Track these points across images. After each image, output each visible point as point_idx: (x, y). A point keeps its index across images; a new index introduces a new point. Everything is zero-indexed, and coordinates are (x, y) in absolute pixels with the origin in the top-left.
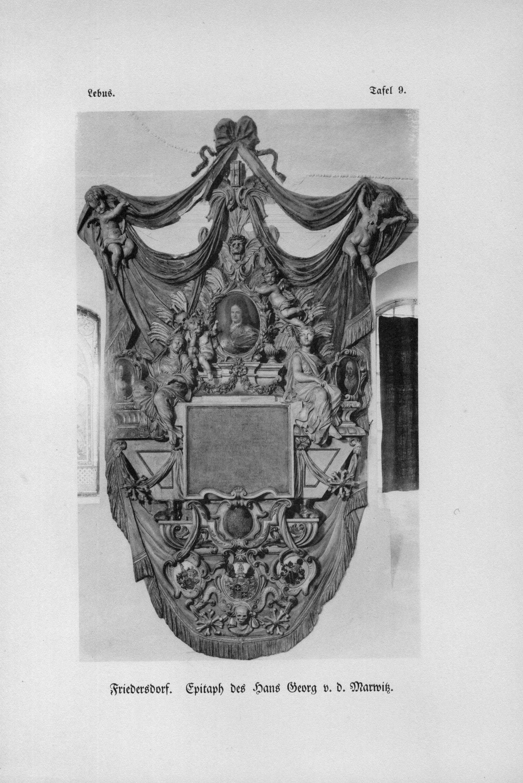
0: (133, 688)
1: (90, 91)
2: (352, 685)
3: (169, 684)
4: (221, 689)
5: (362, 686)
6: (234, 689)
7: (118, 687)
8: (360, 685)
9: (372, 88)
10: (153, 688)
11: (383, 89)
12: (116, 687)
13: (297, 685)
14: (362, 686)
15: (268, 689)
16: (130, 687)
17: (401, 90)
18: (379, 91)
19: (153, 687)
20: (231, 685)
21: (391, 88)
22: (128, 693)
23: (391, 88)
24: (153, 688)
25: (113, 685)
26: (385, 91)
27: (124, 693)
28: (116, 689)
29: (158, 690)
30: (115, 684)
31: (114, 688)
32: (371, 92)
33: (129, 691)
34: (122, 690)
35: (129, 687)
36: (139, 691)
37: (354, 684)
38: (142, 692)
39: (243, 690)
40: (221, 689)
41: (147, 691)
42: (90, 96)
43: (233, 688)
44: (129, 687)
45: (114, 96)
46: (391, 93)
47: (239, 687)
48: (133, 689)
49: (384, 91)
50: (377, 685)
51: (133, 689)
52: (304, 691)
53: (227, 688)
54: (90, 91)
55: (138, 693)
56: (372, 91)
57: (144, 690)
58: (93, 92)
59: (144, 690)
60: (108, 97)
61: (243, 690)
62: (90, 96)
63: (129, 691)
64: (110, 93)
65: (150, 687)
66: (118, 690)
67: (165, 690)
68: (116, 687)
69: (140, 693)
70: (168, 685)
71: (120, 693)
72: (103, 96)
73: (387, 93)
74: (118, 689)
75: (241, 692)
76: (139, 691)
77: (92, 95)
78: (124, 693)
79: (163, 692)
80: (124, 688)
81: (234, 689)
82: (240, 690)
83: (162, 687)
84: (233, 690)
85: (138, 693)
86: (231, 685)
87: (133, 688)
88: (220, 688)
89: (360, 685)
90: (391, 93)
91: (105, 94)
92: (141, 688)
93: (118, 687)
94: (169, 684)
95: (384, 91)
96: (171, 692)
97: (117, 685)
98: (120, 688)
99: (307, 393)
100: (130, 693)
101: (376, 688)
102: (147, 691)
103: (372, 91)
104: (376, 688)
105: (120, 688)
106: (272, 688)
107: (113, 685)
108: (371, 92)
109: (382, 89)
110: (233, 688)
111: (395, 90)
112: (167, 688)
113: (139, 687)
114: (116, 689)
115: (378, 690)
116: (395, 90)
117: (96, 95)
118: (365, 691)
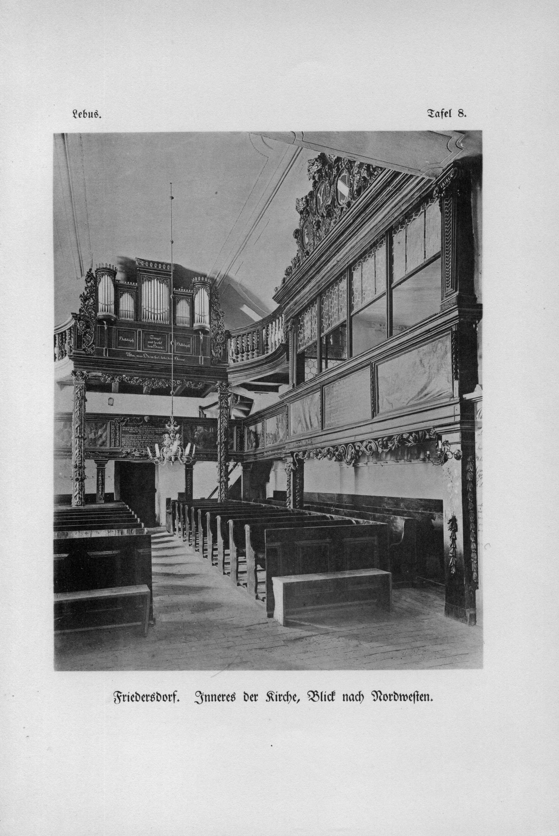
0: (138, 697)
1: (75, 111)
2: (374, 693)
3: (176, 691)
4: (361, 697)
5: (381, 694)
6: (254, 697)
7: (122, 694)
8: (379, 693)
9: (430, 111)
10: (159, 696)
11: (442, 112)
12: (119, 695)
13: (420, 694)
14: (381, 694)
15: (324, 697)
16: (135, 695)
17: (461, 113)
18: (437, 114)
19: (139, 695)
20: (245, 693)
21: (450, 111)
22: (133, 701)
23: (450, 111)
24: (159, 696)
25: (117, 693)
26: (444, 114)
27: (128, 701)
28: (119, 696)
29: (165, 699)
30: (119, 692)
31: (118, 696)
32: (429, 115)
33: (134, 699)
34: (126, 698)
35: (133, 695)
36: (145, 699)
37: (376, 692)
38: (147, 701)
39: (233, 699)
40: (361, 697)
41: (153, 699)
42: (75, 117)
43: (246, 696)
44: (133, 695)
45: (100, 117)
46: (450, 116)
47: (229, 695)
48: (138, 697)
49: (445, 114)
50: (403, 695)
51: (138, 697)
52: (386, 700)
53: (240, 696)
54: (75, 111)
55: (144, 701)
56: (430, 114)
57: (149, 698)
58: (78, 113)
59: (149, 698)
60: (94, 118)
61: (233, 699)
62: (75, 117)
63: (134, 699)
64: (96, 113)
65: (156, 695)
66: (122, 698)
67: (172, 698)
68: (119, 695)
69: (146, 701)
70: (175, 693)
71: (124, 701)
72: (89, 117)
73: (446, 116)
74: (122, 697)
75: (231, 701)
76: (145, 699)
77: (77, 116)
78: (128, 701)
79: (170, 701)
80: (128, 696)
81: (254, 697)
82: (230, 698)
83: (169, 695)
84: (246, 698)
85: (252, 701)
86: (245, 693)
87: (138, 697)
88: (360, 696)
89: (379, 693)
90: (450, 116)
91: (91, 115)
92: (222, 695)
93: (122, 694)
94: (176, 691)
95: (445, 114)
96: (178, 701)
97: (121, 693)
98: (123, 696)
99: (422, 400)
100: (135, 702)
101: (402, 697)
102: (153, 699)
103: (430, 114)
104: (402, 697)
105: (123, 696)
106: (214, 697)
107: (117, 693)
108: (429, 115)
109: (440, 112)
110: (246, 696)
111: (455, 113)
112: (174, 695)
113: (252, 695)
114: (119, 696)
115: (404, 700)
116: (455, 113)
117: (82, 116)
118: (350, 700)
